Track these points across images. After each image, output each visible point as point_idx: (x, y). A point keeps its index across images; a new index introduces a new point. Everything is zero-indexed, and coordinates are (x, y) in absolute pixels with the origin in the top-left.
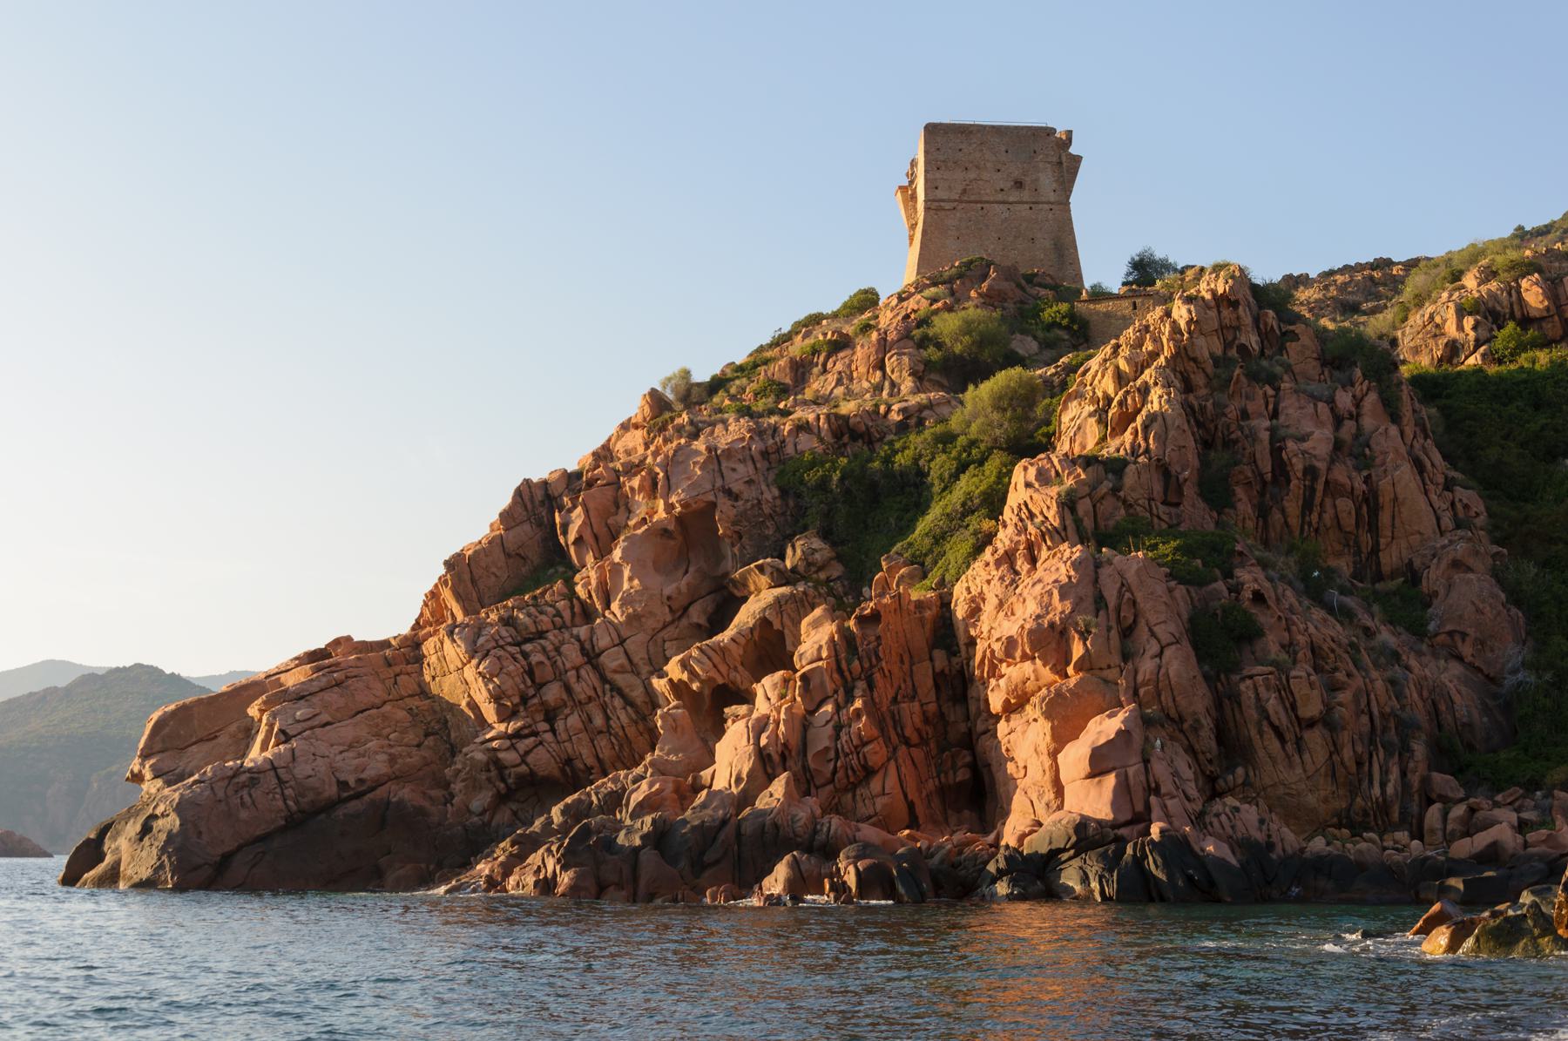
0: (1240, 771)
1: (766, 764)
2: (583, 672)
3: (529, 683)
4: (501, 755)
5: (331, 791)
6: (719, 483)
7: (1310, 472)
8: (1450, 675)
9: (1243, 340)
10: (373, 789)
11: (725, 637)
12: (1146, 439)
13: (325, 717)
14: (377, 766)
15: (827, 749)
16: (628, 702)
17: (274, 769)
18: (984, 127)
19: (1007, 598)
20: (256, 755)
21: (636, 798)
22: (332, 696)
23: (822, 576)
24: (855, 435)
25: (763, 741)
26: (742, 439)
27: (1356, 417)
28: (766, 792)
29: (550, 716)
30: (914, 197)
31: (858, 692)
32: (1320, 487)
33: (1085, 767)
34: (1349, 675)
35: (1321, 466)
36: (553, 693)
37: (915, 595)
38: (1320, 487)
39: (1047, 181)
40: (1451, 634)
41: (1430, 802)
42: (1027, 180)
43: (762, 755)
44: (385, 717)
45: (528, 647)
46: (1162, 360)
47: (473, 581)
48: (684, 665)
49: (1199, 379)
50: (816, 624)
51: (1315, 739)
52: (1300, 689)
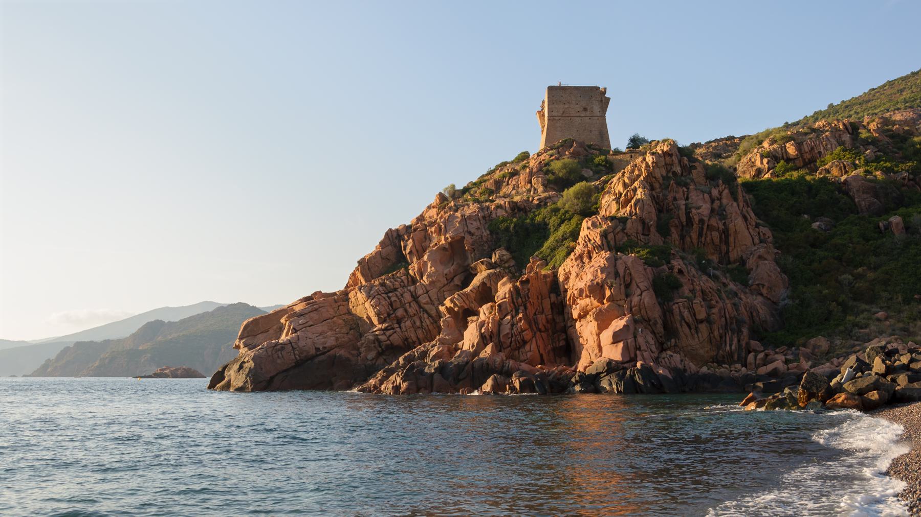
0: (673, 340)
1: (484, 340)
5: (313, 352)
7: (701, 221)
8: (757, 301)
9: (674, 169)
11: (468, 290)
13: (311, 323)
14: (331, 342)
16: (430, 316)
20: (284, 338)
21: (433, 353)
22: (314, 315)
23: (506, 265)
24: (520, 209)
25: (483, 331)
27: (720, 199)
29: (399, 322)
30: (543, 115)
31: (520, 311)
32: (705, 227)
33: (611, 340)
35: (706, 219)
36: (400, 313)
38: (705, 227)
39: (597, 108)
40: (758, 285)
41: (750, 352)
44: (334, 322)
45: (390, 294)
48: (452, 301)
49: (657, 185)
50: (504, 284)
52: (697, 308)
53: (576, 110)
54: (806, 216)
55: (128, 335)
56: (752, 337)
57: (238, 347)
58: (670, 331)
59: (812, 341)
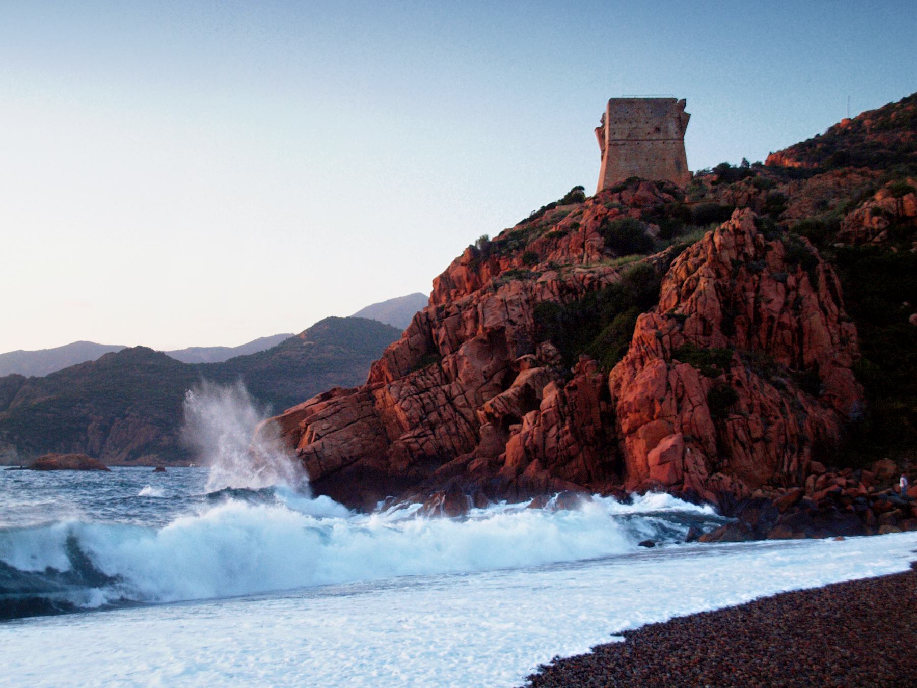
0: (726, 461)
4: (412, 445)
5: (339, 462)
6: (507, 317)
7: (771, 319)
8: (825, 416)
9: (746, 251)
10: (356, 460)
11: (509, 392)
13: (334, 428)
15: (553, 448)
16: (467, 421)
17: (316, 452)
18: (640, 99)
22: (336, 417)
23: (553, 362)
24: (569, 290)
27: (796, 289)
29: (432, 426)
31: (567, 422)
32: (775, 325)
35: (776, 316)
36: (433, 417)
38: (775, 325)
39: (673, 127)
40: (829, 396)
41: (810, 474)
42: (662, 127)
43: (526, 450)
45: (422, 396)
47: (396, 362)
49: (724, 272)
50: (550, 391)
51: (758, 447)
52: (752, 425)
54: (906, 304)
56: (814, 457)
58: (723, 450)
59: (878, 464)
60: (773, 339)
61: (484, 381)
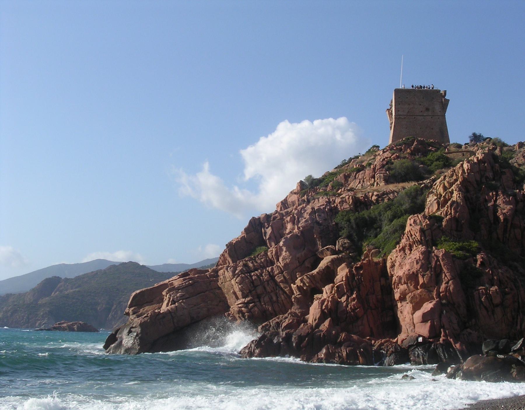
0: (474, 320)
1: (323, 316)
2: (270, 282)
3: (252, 286)
11: (315, 272)
12: (451, 209)
13: (187, 296)
16: (285, 292)
19: (402, 263)
20: (164, 308)
21: (284, 324)
25: (324, 307)
26: (323, 205)
28: (323, 325)
29: (259, 297)
30: (392, 114)
32: (509, 225)
34: (511, 289)
36: (259, 290)
37: (376, 260)
38: (509, 225)
39: (438, 107)
43: (322, 311)
46: (458, 182)
48: (302, 281)
50: (342, 269)
51: (498, 310)
53: (420, 112)
55: (28, 290)
57: (128, 314)
58: (471, 313)
60: (507, 235)
61: (298, 264)
